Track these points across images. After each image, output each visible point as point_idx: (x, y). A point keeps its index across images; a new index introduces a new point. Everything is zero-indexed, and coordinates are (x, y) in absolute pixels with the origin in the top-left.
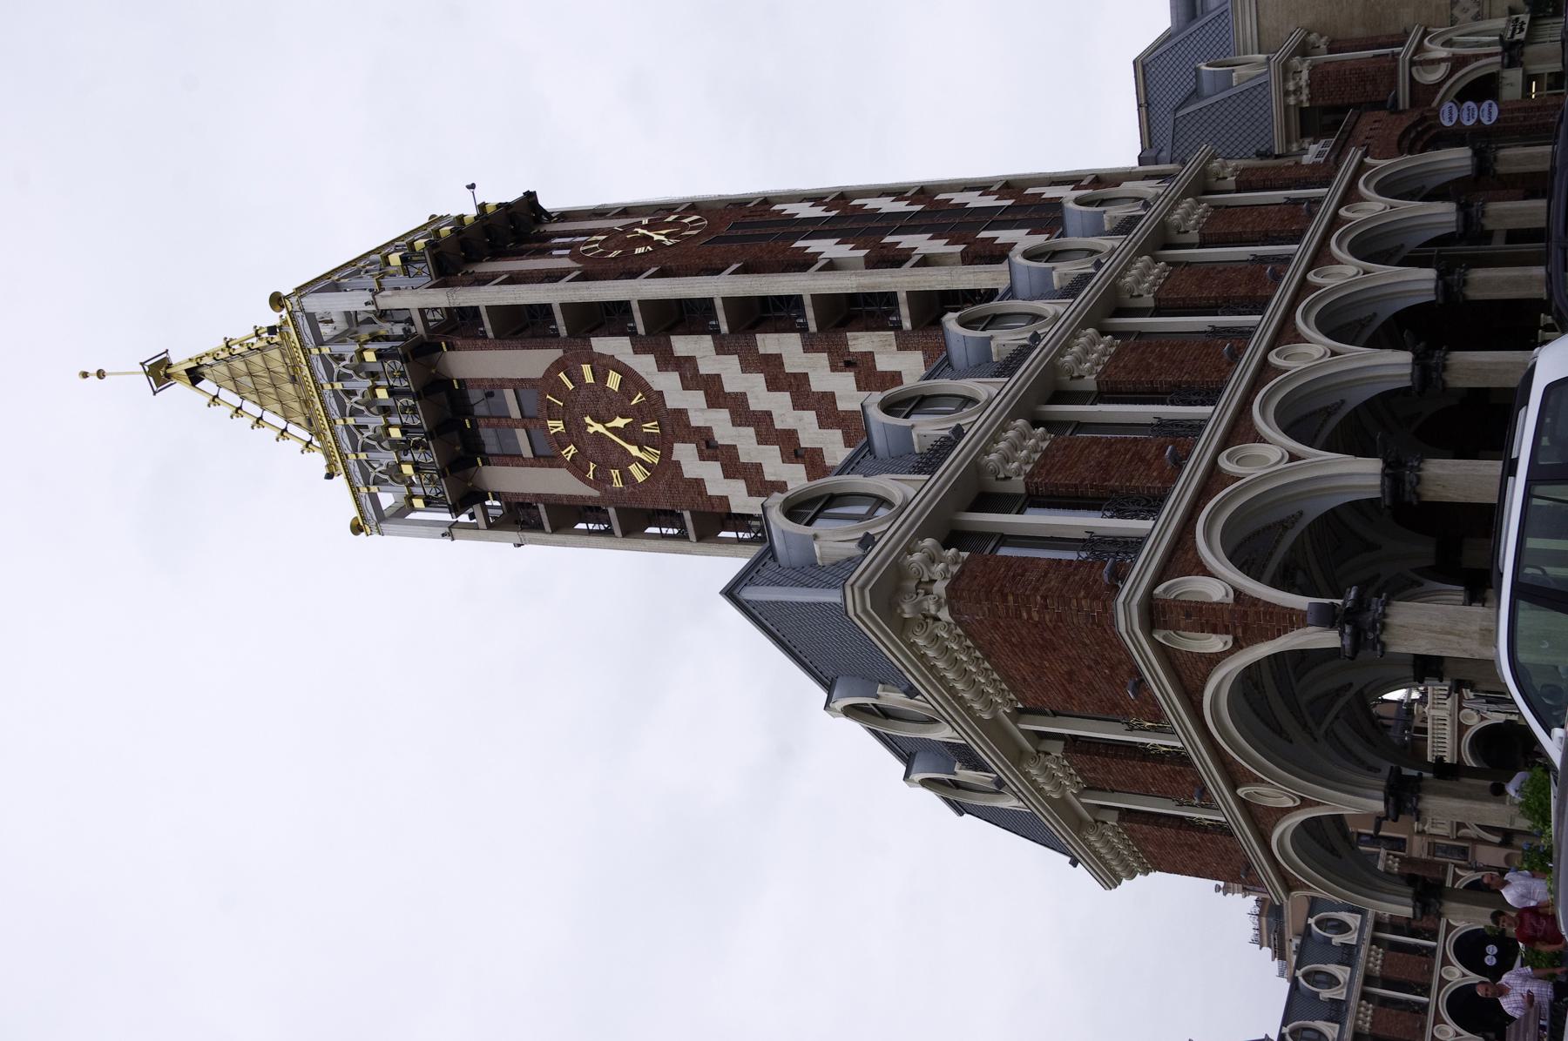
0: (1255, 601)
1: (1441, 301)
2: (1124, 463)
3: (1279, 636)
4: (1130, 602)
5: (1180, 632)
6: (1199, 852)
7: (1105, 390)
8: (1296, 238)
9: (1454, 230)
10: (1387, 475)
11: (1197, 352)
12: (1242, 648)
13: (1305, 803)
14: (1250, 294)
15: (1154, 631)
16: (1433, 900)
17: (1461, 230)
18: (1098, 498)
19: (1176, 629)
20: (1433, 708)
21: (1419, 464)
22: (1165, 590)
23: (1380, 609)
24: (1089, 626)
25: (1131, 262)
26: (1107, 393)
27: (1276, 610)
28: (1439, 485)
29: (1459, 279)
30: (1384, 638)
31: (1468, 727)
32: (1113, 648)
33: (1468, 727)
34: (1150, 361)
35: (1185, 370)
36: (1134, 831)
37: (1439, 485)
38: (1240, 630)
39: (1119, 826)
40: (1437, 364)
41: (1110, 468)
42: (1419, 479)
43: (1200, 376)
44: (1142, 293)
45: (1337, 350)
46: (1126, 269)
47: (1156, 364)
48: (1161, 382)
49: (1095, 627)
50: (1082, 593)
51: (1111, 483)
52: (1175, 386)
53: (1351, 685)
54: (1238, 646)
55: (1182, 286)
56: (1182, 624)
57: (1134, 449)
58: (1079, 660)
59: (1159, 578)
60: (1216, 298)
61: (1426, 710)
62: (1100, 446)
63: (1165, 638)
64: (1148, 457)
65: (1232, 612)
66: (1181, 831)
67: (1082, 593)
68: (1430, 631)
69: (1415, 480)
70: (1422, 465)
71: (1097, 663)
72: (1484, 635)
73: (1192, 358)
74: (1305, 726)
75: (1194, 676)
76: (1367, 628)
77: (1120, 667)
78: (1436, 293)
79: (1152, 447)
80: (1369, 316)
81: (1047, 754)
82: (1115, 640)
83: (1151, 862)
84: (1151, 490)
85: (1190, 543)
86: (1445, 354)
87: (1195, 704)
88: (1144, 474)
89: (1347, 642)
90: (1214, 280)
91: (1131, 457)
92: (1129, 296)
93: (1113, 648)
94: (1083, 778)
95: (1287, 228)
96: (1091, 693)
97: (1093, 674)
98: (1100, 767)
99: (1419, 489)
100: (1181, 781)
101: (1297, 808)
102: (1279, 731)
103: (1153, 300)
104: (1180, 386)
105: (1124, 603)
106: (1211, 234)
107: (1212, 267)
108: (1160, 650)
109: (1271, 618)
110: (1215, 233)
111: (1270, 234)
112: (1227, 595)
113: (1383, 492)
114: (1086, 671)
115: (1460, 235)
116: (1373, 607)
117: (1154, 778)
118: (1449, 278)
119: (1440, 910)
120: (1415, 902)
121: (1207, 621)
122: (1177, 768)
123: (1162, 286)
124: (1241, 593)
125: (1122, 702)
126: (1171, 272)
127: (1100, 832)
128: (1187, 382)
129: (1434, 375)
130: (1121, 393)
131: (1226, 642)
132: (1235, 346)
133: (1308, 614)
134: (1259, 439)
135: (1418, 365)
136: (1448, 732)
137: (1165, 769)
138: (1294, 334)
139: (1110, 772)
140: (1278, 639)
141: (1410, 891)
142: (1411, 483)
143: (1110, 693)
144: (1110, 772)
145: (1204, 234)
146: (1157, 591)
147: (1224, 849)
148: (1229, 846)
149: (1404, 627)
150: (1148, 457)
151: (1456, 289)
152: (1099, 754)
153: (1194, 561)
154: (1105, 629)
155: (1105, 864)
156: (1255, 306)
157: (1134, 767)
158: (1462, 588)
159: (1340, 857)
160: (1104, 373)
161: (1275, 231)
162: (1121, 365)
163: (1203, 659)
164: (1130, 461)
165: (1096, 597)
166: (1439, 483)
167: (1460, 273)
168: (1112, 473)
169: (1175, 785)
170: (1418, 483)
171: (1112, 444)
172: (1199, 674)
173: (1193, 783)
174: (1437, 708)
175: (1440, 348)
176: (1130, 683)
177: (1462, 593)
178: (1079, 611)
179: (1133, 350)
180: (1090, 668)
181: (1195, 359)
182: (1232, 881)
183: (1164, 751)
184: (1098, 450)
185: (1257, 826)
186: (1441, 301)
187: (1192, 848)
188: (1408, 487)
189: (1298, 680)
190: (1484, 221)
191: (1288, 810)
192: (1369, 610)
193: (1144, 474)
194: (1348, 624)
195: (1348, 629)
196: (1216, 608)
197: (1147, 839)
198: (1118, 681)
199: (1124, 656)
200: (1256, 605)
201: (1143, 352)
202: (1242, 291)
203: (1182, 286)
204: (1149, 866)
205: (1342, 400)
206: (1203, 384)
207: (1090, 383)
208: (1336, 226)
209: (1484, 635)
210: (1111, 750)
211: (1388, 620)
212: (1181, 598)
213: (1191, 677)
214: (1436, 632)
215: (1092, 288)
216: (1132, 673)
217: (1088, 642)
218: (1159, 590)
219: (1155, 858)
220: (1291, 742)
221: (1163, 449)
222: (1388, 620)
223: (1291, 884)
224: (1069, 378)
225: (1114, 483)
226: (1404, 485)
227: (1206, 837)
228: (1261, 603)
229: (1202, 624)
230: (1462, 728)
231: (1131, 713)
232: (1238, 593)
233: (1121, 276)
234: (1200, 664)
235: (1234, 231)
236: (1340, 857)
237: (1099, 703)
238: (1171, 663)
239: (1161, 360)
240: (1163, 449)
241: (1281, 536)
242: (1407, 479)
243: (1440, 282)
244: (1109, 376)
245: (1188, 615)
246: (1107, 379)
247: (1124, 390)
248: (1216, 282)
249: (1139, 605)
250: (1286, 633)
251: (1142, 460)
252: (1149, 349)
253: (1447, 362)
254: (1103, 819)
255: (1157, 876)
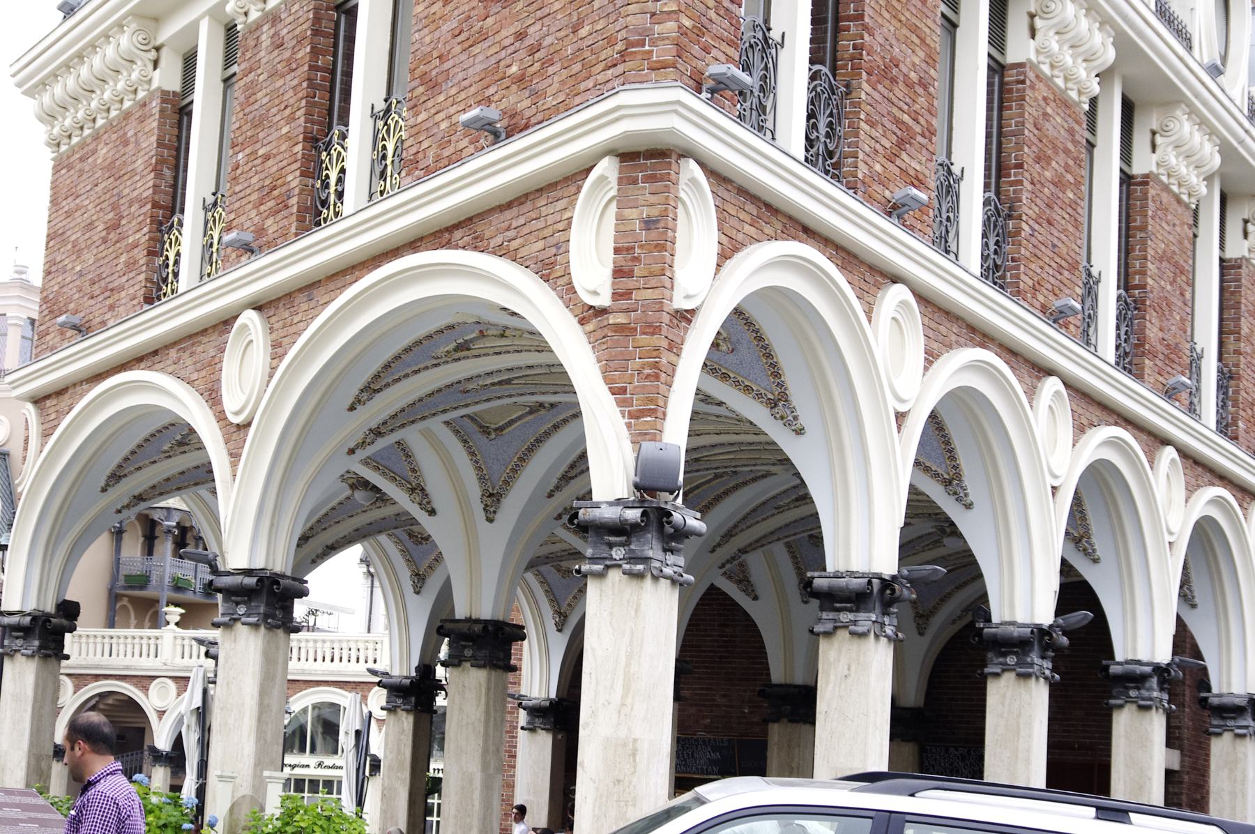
0: (675, 347)
1: (1114, 669)
2: (895, 110)
3: (613, 392)
4: (676, 112)
5: (613, 208)
6: (105, 240)
7: (1007, 79)
8: (1226, 427)
9: (1215, 690)
10: (870, 583)
11: (1065, 250)
12: (582, 322)
13: (236, 432)
14: (1147, 347)
15: (617, 159)
16: (37, 643)
17: (1214, 701)
18: (835, 59)
19: (623, 201)
20: (175, 638)
21: (886, 636)
22: (693, 181)
23: (668, 571)
24: (623, 34)
25: (1212, 132)
26: (1002, 84)
27: (663, 388)
28: (849, 669)
29: (1151, 699)
30: (615, 575)
31: (145, 689)
32: (571, 82)
33: (145, 689)
34: (1054, 163)
35: (1037, 227)
36: (142, 120)
37: (849, 669)
38: (621, 319)
39: (151, 94)
40: (1032, 665)
41: (887, 82)
42: (863, 635)
43: (1028, 254)
44: (1158, 151)
45: (1059, 494)
46: (1203, 123)
47: (1048, 174)
48: (1020, 182)
49: (619, 47)
50: (687, 23)
51: (865, 86)
52: (1011, 209)
53: (432, 512)
54: (589, 315)
55: (1164, 225)
56: (629, 213)
57: (918, 129)
58: (539, 14)
59: (718, 176)
60: (1142, 287)
61: (172, 626)
62: (924, 65)
63: (602, 179)
64: (904, 156)
65: (659, 305)
66: (149, 206)
67: (687, 23)
68: (629, 657)
69: (860, 629)
70: (884, 640)
71: (534, 50)
72: (625, 745)
73: (1056, 241)
74: (377, 433)
75: (511, 234)
76: (632, 547)
77: (527, 93)
78: (1128, 662)
79: (920, 163)
80: (1094, 551)
81: (156, 64)
82: (590, 84)
83: (73, 151)
84: (850, 160)
85: (768, 230)
86: (1046, 678)
87: (447, 235)
88: (878, 147)
89: (609, 514)
90: (1171, 284)
91: (903, 123)
92: (1155, 127)
93: (571, 82)
94: (258, 26)
95: (1241, 413)
96: (460, 38)
97: (506, 42)
98: (287, 54)
99: (843, 635)
100: (262, 208)
101: (221, 417)
102: (371, 389)
103: (1146, 171)
104: (1010, 217)
105: (678, 102)
106: (1239, 280)
107: (1185, 276)
108: (574, 175)
109: (648, 376)
110: (1240, 287)
111: (1232, 382)
112: (688, 297)
113: (837, 575)
114: (512, 30)
115: (1206, 699)
116: (671, 558)
117: (267, 157)
118: (1154, 681)
119: (18, 656)
120: (29, 614)
121: (637, 259)
122: (294, 201)
123: (1166, 188)
124: (690, 322)
125: (441, 98)
126: (1187, 206)
127: (138, 56)
128: (1018, 232)
129: (1011, 660)
130: (1001, 109)
131: (595, 293)
132: (1071, 319)
133: (658, 445)
134: (931, 357)
135: (1032, 632)
136: (145, 664)
137: (290, 178)
138: (1085, 421)
139: (274, 75)
140: (606, 388)
141: (50, 607)
142: (855, 622)
143: (461, 76)
144: (274, 75)
145: (1240, 267)
146: (692, 164)
147: (116, 284)
148: (123, 294)
149: (636, 611)
150: (904, 156)
151: (1133, 693)
152: (315, 52)
153: (740, 237)
154: (615, 65)
155: (67, 66)
156: (1126, 354)
157: (292, 119)
158: (553, 695)
159: (104, 490)
160: (1037, 77)
161: (1237, 392)
162: (1049, 110)
163: (553, 250)
164: (898, 122)
165: (681, 51)
166: (853, 668)
167: (1161, 700)
168: (880, 87)
169: (254, 197)
170: (852, 633)
171: (925, 88)
172: (518, 241)
173: (260, 231)
174: (175, 645)
175: (1054, 670)
176: (492, 113)
177: (543, 696)
178: (653, 14)
179: (1071, 132)
180: (520, 36)
181: (1054, 246)
182: (45, 300)
183: (327, 176)
184: (917, 61)
185: (174, 344)
186: (1114, 669)
187: (114, 226)
188: (845, 617)
189: (447, 423)
190: (1227, 736)
191: (213, 397)
192: (665, 551)
193: (878, 147)
194: (643, 514)
195: (633, 515)
196: (663, 274)
197: (126, 143)
198: (492, 90)
199: (551, 102)
200: (670, 350)
201: (1067, 151)
202: (1153, 333)
203: (1164, 225)
204: (63, 148)
205: (971, 504)
206: (1013, 260)
207: (1019, 49)
208: (1239, 495)
209: (625, 745)
210: (323, 79)
211: (648, 581)
212: (680, 211)
213: (508, 229)
214: (628, 665)
215: (1181, 59)
216: (513, 116)
217: (583, 32)
218: (692, 169)
219: (82, 160)
220: (352, 408)
221: (916, 182)
222: (648, 581)
223: (48, 403)
224: (1033, 10)
225: (865, 90)
226: (851, 611)
227: (140, 255)
228: (673, 358)
229: (630, 249)
230: (144, 681)
231: (417, 114)
232: (686, 317)
233: (1192, 111)
234: (540, 245)
235: (1243, 319)
236: (104, 490)
237: (435, 54)
238: (540, 190)
239: (1054, 184)
240: (916, 182)
241: (759, 396)
242: (862, 616)
243: (1148, 669)
244: (1032, 87)
245: (649, 224)
246: (1028, 82)
247: (1006, 113)
248: (1169, 287)
249: (672, 132)
250: (620, 403)
251: (901, 144)
252: (1071, 163)
253: (1034, 679)
254: (162, 63)
255: (45, 160)
